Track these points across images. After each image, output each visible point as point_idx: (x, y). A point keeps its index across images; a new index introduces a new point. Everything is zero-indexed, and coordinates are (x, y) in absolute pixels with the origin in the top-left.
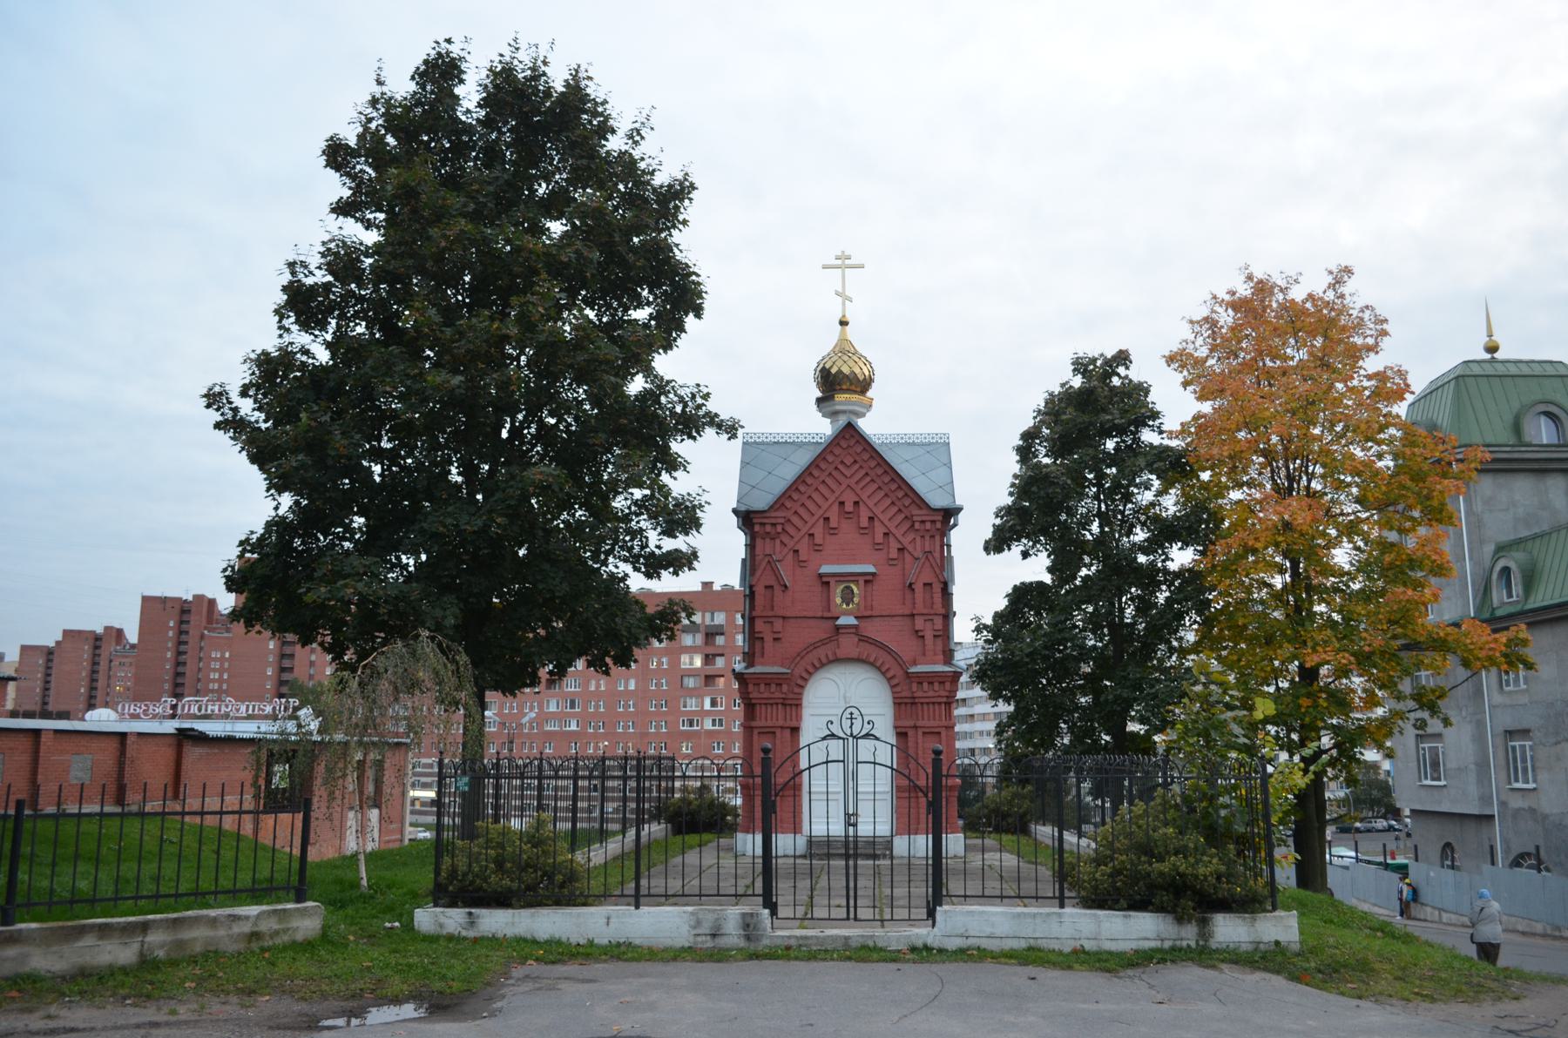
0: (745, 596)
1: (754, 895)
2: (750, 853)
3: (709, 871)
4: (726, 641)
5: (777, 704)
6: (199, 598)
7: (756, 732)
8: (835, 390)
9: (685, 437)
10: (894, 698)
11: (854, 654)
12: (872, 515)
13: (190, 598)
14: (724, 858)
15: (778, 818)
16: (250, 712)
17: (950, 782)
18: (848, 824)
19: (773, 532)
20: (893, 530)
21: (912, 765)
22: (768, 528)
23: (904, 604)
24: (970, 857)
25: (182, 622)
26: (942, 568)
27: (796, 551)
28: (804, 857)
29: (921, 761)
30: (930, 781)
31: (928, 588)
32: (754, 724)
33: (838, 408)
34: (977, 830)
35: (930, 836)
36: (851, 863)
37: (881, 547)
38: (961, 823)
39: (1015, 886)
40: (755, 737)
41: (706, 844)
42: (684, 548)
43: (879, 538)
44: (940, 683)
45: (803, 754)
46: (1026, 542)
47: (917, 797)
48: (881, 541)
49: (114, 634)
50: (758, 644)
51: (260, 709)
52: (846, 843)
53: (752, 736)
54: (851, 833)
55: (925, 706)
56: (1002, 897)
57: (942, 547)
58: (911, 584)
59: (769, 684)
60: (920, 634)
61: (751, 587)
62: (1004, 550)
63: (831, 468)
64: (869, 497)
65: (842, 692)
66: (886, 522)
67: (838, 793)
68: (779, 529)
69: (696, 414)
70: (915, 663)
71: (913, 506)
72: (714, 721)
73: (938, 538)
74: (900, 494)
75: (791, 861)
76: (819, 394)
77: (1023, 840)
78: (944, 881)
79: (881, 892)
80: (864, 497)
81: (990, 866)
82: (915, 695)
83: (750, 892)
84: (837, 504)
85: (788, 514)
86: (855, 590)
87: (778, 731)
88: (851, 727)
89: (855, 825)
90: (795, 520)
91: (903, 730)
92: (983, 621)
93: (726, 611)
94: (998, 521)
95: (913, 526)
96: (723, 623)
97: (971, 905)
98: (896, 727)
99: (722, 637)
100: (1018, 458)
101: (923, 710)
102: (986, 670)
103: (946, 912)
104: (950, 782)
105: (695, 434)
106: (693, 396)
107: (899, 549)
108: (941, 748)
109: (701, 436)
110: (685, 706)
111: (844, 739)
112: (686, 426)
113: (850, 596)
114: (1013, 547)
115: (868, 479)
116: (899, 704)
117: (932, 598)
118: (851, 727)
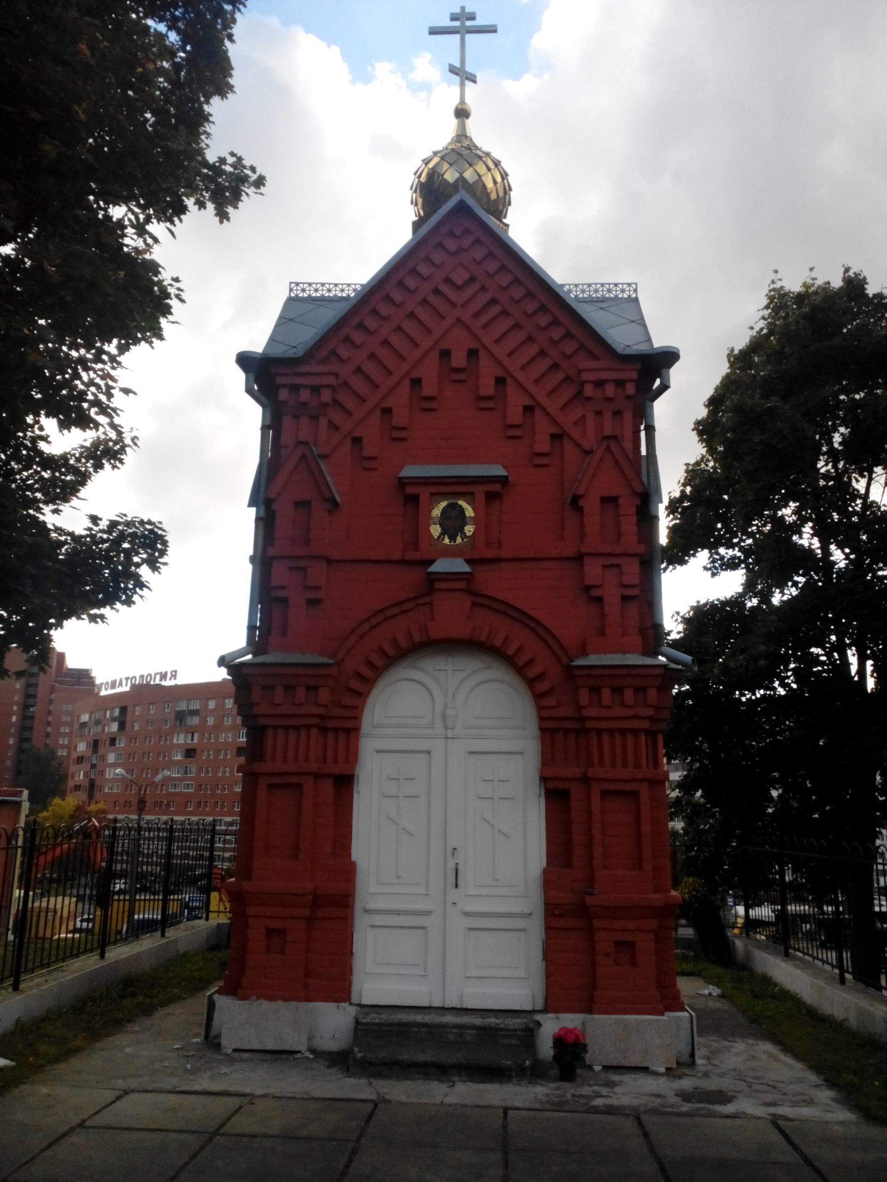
5: (308, 727)
12: (501, 373)
27: (357, 441)
32: (259, 767)
60: (595, 593)
65: (439, 708)
70: (584, 653)
82: (586, 713)
84: (436, 354)
86: (469, 512)
87: (308, 784)
91: (561, 785)
95: (580, 393)
98: (544, 779)
101: (601, 746)
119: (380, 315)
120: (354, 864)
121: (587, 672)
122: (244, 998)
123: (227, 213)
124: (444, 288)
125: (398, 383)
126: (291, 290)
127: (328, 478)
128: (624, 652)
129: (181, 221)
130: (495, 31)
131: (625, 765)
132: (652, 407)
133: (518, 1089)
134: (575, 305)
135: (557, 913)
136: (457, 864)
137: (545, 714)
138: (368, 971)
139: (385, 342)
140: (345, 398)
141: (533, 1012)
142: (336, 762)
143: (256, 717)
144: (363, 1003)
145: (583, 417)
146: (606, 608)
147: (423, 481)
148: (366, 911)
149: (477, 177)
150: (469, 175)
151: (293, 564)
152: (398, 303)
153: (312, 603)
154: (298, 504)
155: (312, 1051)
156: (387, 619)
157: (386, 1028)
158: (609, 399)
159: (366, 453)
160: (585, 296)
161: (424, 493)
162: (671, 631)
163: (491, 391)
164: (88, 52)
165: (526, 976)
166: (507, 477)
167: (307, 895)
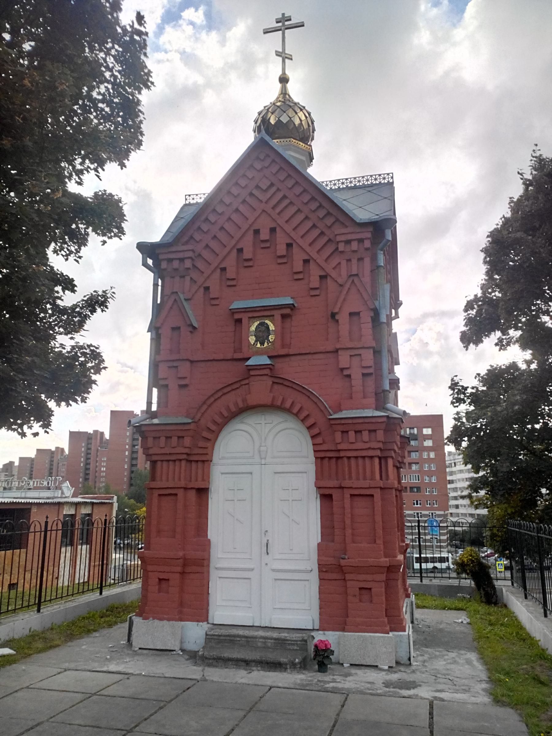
5: (180, 460)
6: (96, 432)
12: (289, 241)
13: (92, 432)
16: (35, 485)
20: (314, 255)
25: (88, 444)
27: (207, 289)
44: (370, 431)
48: (301, 269)
49: (60, 451)
51: (40, 483)
60: (346, 372)
66: (323, 264)
82: (340, 447)
86: (272, 327)
87: (181, 493)
91: (327, 492)
116: (322, 458)
120: (209, 540)
122: (145, 618)
123: (124, 163)
124: (255, 192)
125: (229, 253)
126: (186, 199)
128: (363, 408)
129: (103, 170)
130: (303, 26)
131: (365, 478)
133: (290, 676)
134: (329, 195)
135: (324, 570)
136: (268, 540)
138: (218, 604)
139: (222, 228)
140: (200, 264)
141: (313, 630)
142: (197, 480)
143: (151, 455)
144: (215, 623)
145: (339, 263)
147: (280, 307)
148: (216, 568)
149: (289, 119)
150: (284, 119)
151: (171, 364)
153: (182, 386)
154: (173, 329)
155: (182, 650)
156: (224, 394)
157: (222, 638)
158: (354, 251)
159: (212, 296)
160: (361, 184)
161: (245, 317)
162: (468, 387)
163: (284, 253)
164: (29, 85)
165: (309, 608)
166: (293, 304)
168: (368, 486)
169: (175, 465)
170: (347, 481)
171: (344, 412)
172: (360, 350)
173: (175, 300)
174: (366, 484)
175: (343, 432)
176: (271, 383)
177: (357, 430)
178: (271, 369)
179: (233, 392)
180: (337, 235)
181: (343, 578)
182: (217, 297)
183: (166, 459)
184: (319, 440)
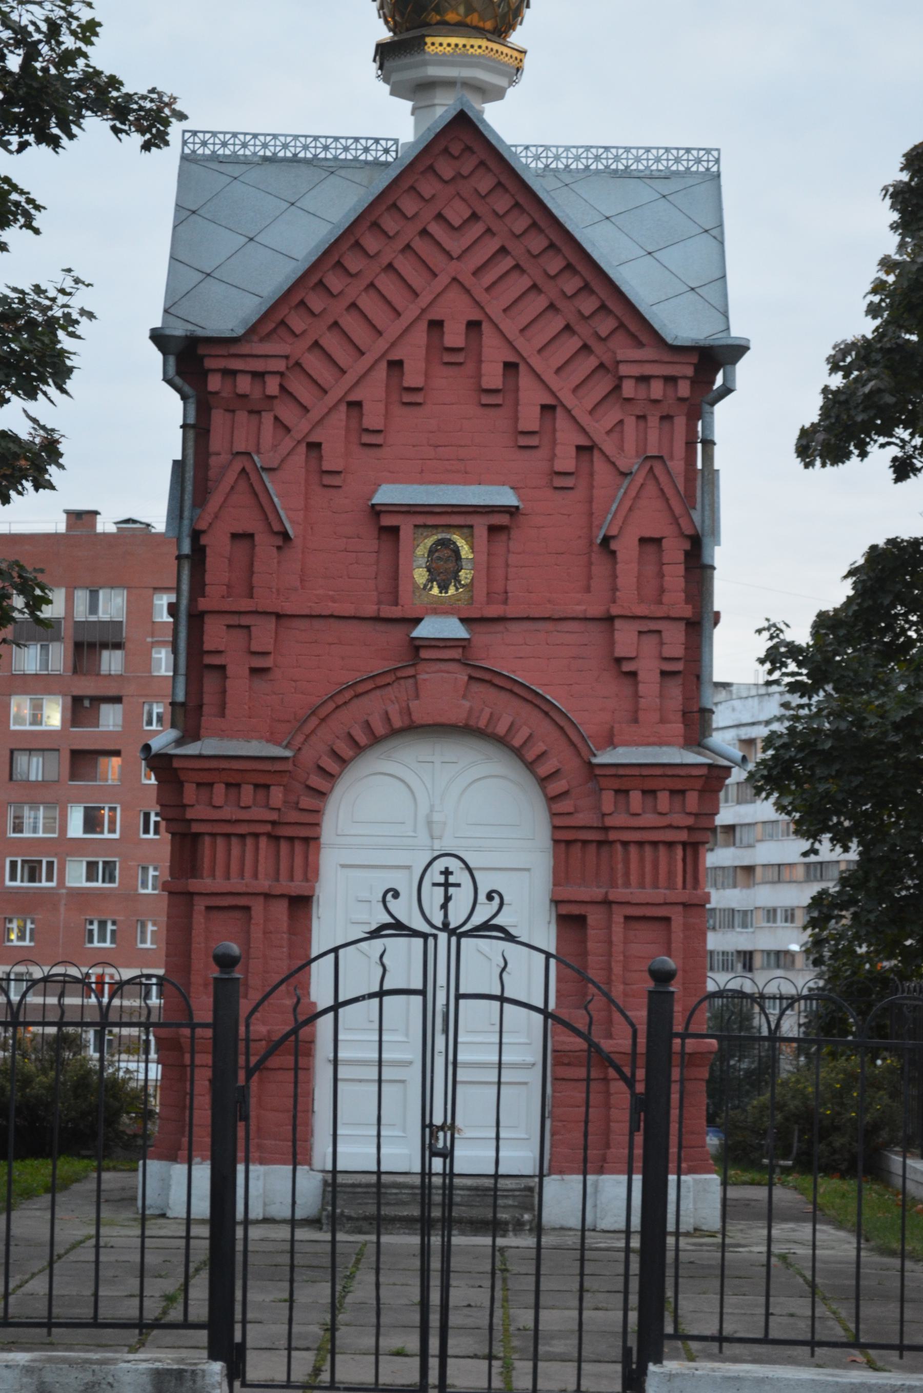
0: (179, 558)
1: (186, 1325)
2: (178, 1210)
3: (72, 1257)
4: (127, 663)
5: (256, 836)
7: (200, 905)
8: (428, 25)
9: (31, 138)
10: (555, 828)
11: (457, 713)
12: (512, 358)
14: (112, 1224)
15: (253, 1128)
17: (691, 1044)
18: (429, 1150)
19: (256, 394)
20: (568, 399)
21: (598, 1004)
22: (244, 384)
23: (588, 589)
24: (737, 1231)
26: (689, 500)
28: (314, 1222)
29: (617, 991)
30: (642, 1040)
31: (651, 549)
32: (195, 885)
33: (434, 72)
34: (753, 1165)
35: (638, 1179)
36: (436, 1240)
37: (533, 441)
38: (713, 1141)
39: (846, 1311)
40: (199, 918)
41: (65, 1187)
42: (23, 430)
43: (530, 418)
44: (673, 792)
45: (321, 973)
46: (906, 435)
47: (606, 1080)
48: (535, 427)
50: (210, 683)
52: (425, 1187)
53: (189, 915)
54: (437, 1164)
55: (633, 850)
56: (813, 1344)
57: (690, 445)
58: (606, 540)
59: (238, 785)
60: (627, 667)
61: (196, 535)
62: (847, 456)
63: (410, 232)
64: (558, 370)
65: (423, 810)
66: (584, 419)
67: (410, 1063)
68: (272, 386)
69: (60, 77)
70: (610, 741)
71: (620, 337)
72: (92, 866)
73: (680, 422)
74: (588, 305)
75: (283, 1232)
76: (385, 35)
77: (872, 1192)
78: (669, 1293)
79: (507, 1318)
80: (494, 309)
81: (783, 1258)
82: (609, 822)
83: (175, 1314)
84: (423, 325)
85: (297, 349)
86: (465, 551)
87: (258, 907)
88: (444, 906)
89: (448, 1154)
90: (314, 363)
91: (575, 910)
92: (788, 636)
93: (128, 588)
94: (837, 381)
95: (618, 388)
96: (120, 616)
97: (736, 1360)
98: (556, 902)
99: (118, 654)
100: (895, 216)
101: (627, 861)
102: (793, 760)
103: (671, 1377)
104: (691, 1044)
105: (56, 131)
106: (54, 29)
107: (579, 448)
108: (671, 963)
109: (71, 136)
110: (18, 828)
111: (425, 936)
112: (34, 109)
113: (451, 565)
114: (872, 449)
115: (507, 263)
116: (568, 843)
117: (661, 575)
118: (444, 906)
119: (346, 270)
121: (612, 771)
127: (276, 500)
128: (661, 744)
131: (655, 886)
132: (712, 413)
137: (560, 822)
146: (641, 687)
147: (487, 510)
152: (372, 254)
156: (357, 696)
159: (326, 466)
166: (517, 507)
167: (260, 1040)
168: (662, 901)
169: (244, 845)
170: (649, 890)
171: (621, 750)
172: (660, 622)
173: (243, 469)
174: (660, 894)
175: (617, 791)
176: (466, 678)
177: (646, 788)
178: (464, 647)
179: (378, 693)
180: (621, 361)
181: (602, 1076)
182: (340, 470)
183: (224, 831)
184: (564, 806)
